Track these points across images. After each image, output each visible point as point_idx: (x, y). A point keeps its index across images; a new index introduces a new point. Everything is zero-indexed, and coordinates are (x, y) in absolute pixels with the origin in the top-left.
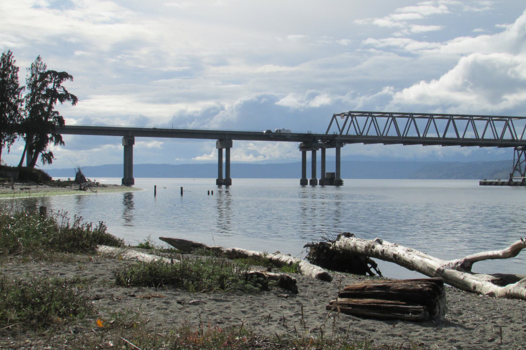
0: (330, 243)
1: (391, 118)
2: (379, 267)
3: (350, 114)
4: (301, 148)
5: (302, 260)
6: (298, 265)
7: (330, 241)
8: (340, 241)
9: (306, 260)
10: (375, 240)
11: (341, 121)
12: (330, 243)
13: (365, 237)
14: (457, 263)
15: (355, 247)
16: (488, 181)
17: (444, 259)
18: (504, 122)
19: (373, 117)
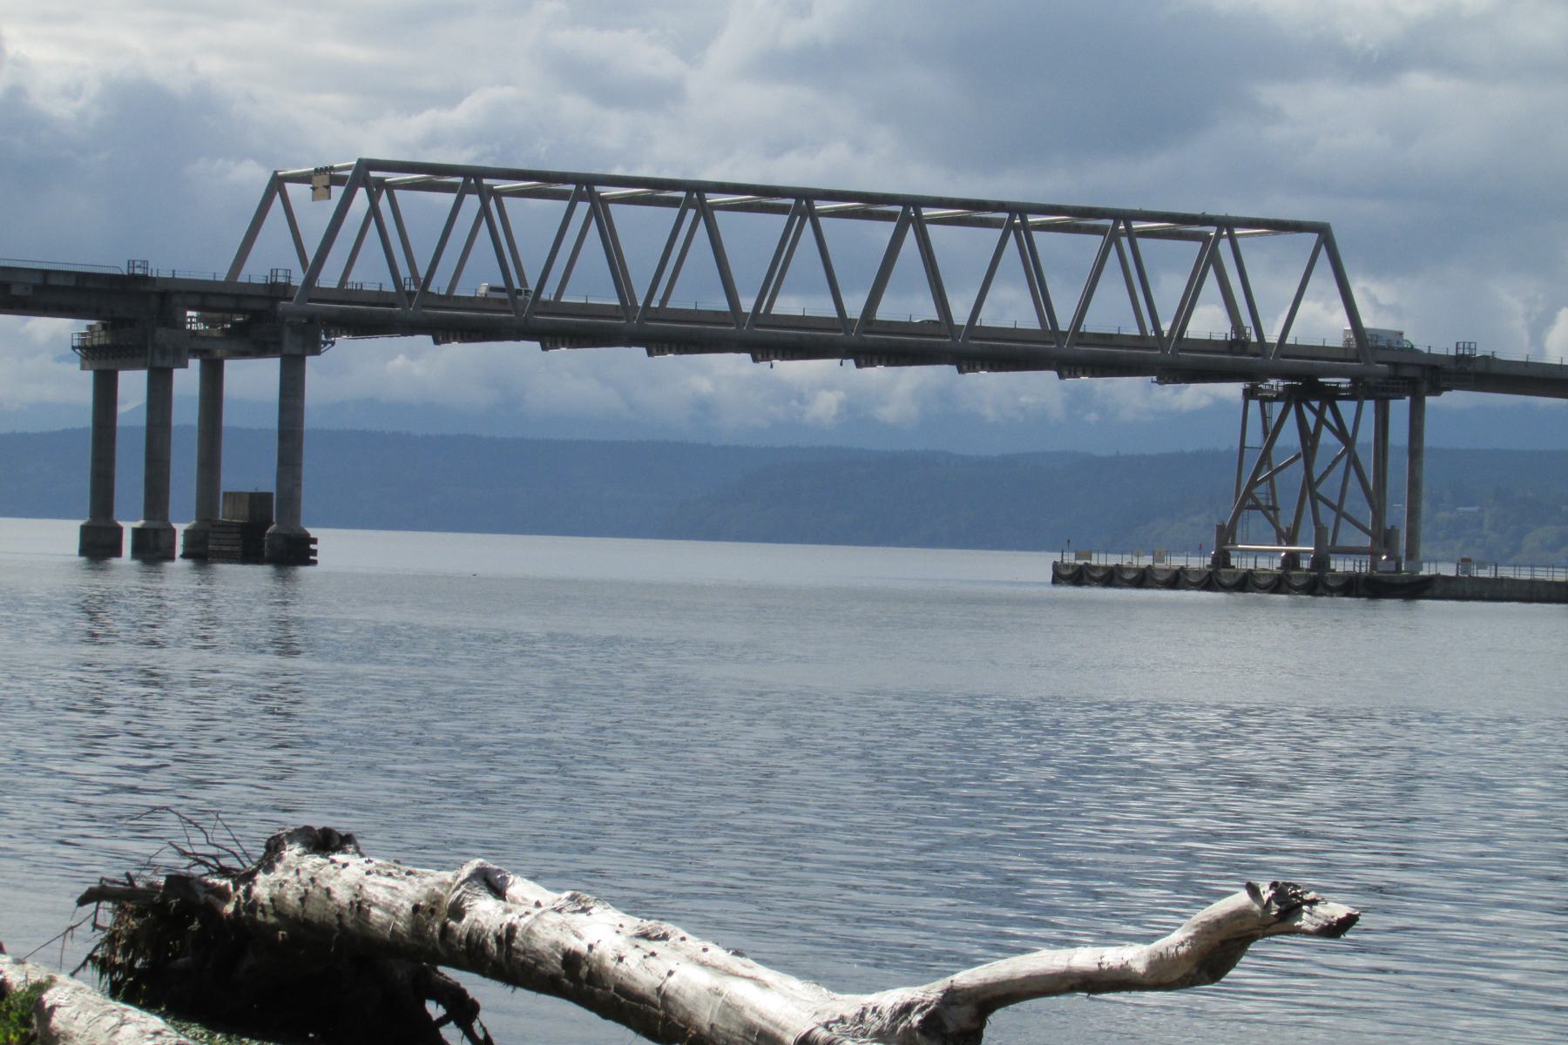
0: (223, 882)
1: (583, 208)
2: (487, 1020)
3: (364, 175)
4: (89, 352)
5: (62, 978)
6: (39, 1004)
7: (224, 872)
8: (279, 873)
9: (92, 973)
10: (466, 872)
11: (314, 213)
12: (223, 882)
13: (406, 858)
14: (907, 1009)
15: (360, 907)
16: (1100, 560)
17: (463, 993)
18: (1197, 246)
19: (486, 194)
